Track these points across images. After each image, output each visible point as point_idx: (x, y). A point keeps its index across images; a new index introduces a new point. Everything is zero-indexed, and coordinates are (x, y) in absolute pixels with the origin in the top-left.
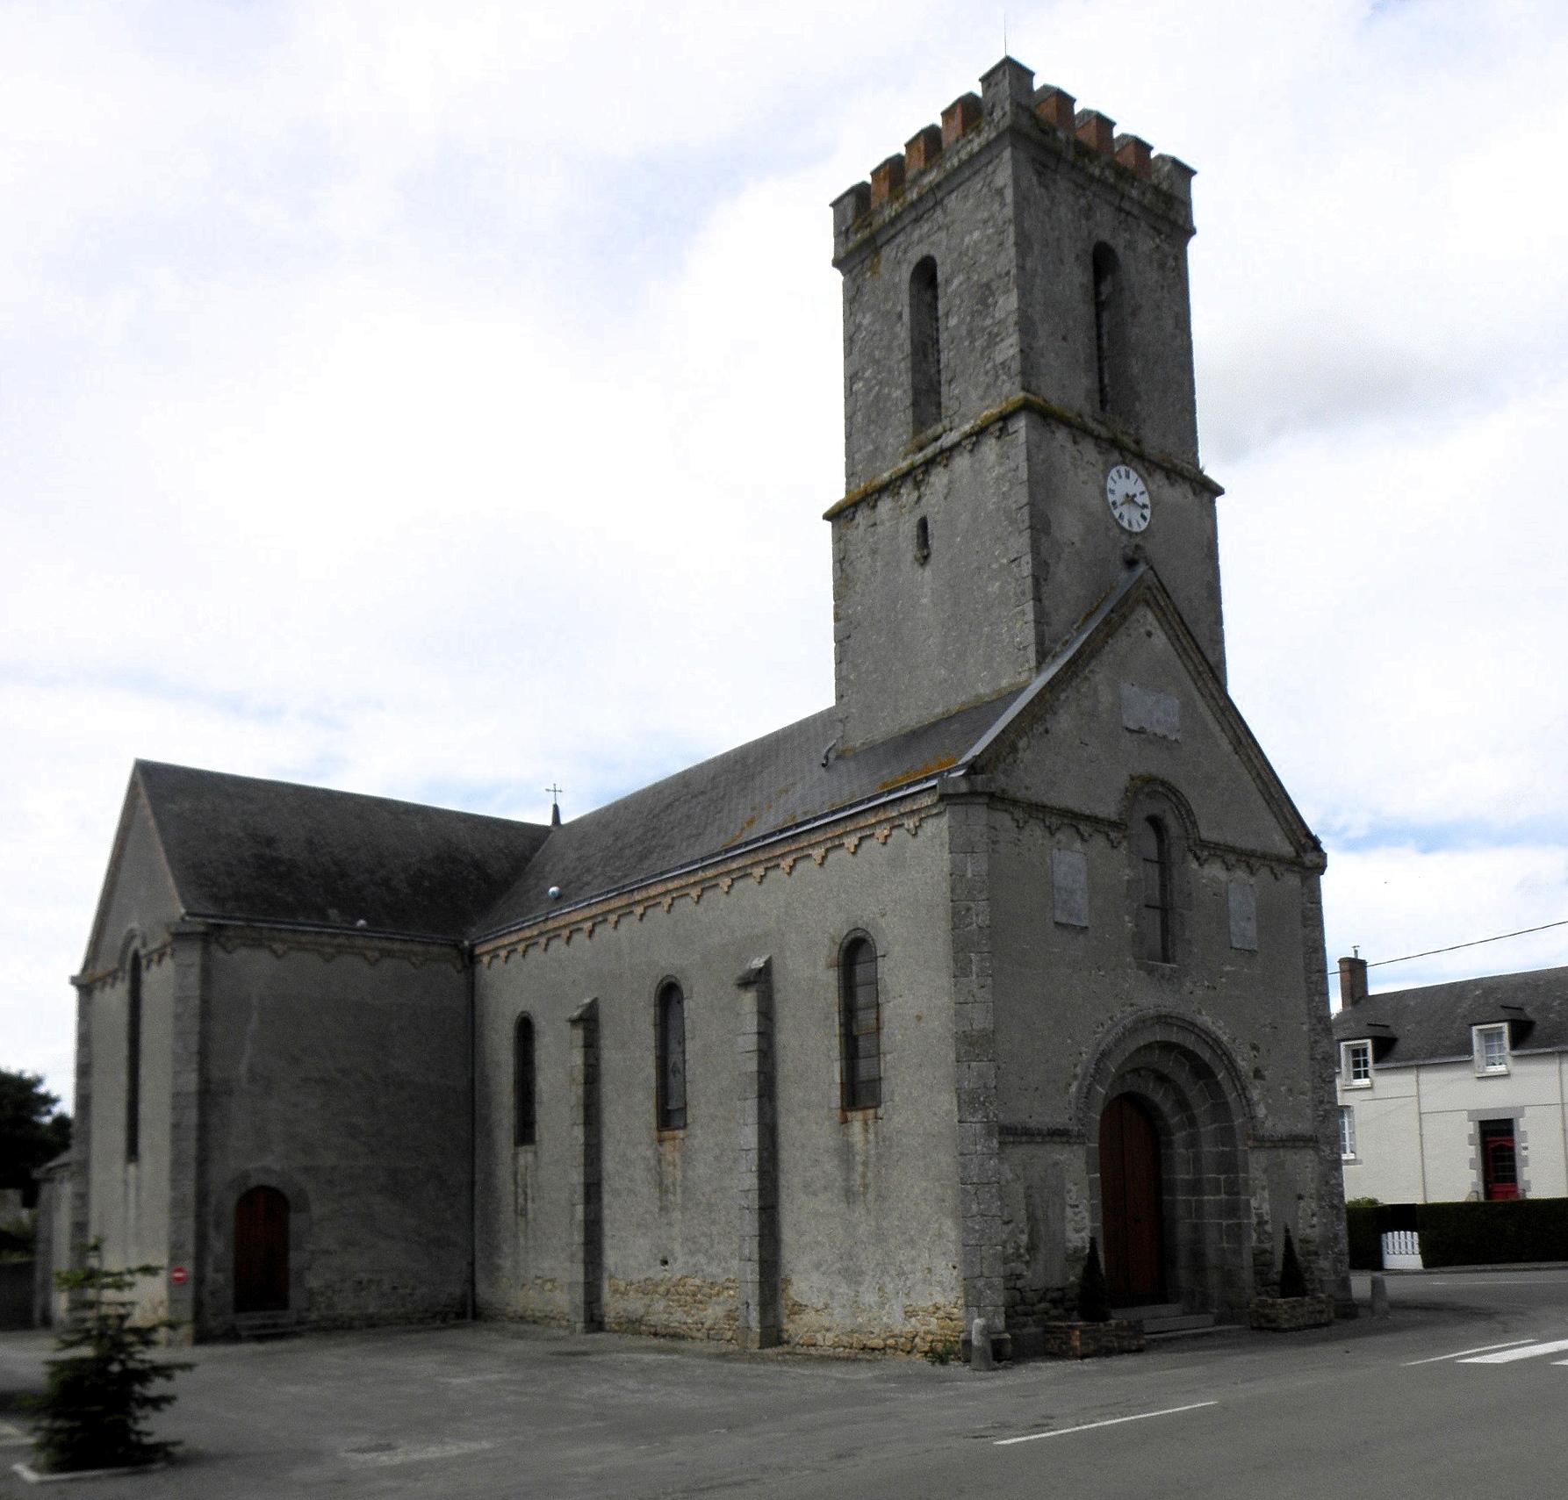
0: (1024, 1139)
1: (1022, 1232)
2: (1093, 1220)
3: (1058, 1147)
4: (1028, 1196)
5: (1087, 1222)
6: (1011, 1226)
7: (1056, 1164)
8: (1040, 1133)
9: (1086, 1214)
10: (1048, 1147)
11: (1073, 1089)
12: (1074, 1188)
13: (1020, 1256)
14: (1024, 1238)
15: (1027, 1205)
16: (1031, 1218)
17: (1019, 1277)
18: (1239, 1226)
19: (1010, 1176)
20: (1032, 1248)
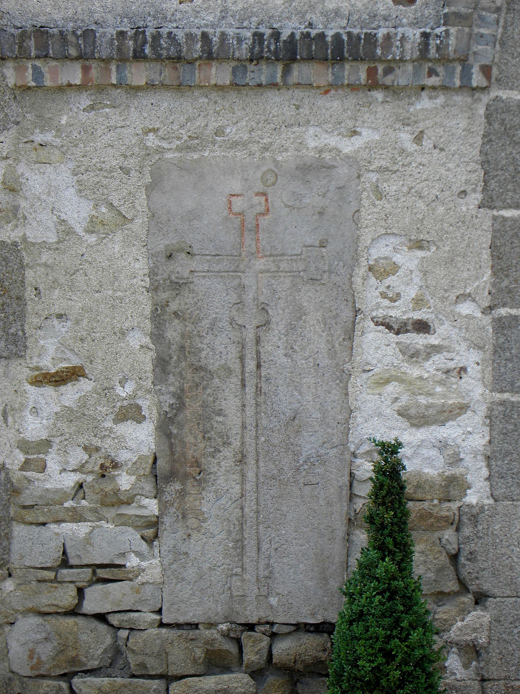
0: (138, 74)
1: (131, 413)
2: (498, 384)
3: (334, 105)
4: (168, 291)
5: (475, 388)
6: (71, 394)
7: (313, 169)
8: (212, 51)
9: (471, 358)
10: (278, 104)
11: (84, 659)
12: (408, 260)
13: (117, 500)
14: (140, 439)
15: (159, 316)
16: (177, 363)
17: (107, 572)
18: (342, 59)
19: (77, 211)
20: (172, 470)
